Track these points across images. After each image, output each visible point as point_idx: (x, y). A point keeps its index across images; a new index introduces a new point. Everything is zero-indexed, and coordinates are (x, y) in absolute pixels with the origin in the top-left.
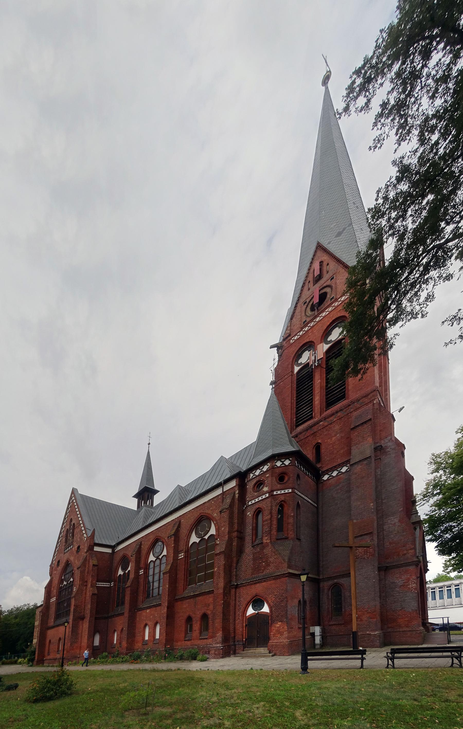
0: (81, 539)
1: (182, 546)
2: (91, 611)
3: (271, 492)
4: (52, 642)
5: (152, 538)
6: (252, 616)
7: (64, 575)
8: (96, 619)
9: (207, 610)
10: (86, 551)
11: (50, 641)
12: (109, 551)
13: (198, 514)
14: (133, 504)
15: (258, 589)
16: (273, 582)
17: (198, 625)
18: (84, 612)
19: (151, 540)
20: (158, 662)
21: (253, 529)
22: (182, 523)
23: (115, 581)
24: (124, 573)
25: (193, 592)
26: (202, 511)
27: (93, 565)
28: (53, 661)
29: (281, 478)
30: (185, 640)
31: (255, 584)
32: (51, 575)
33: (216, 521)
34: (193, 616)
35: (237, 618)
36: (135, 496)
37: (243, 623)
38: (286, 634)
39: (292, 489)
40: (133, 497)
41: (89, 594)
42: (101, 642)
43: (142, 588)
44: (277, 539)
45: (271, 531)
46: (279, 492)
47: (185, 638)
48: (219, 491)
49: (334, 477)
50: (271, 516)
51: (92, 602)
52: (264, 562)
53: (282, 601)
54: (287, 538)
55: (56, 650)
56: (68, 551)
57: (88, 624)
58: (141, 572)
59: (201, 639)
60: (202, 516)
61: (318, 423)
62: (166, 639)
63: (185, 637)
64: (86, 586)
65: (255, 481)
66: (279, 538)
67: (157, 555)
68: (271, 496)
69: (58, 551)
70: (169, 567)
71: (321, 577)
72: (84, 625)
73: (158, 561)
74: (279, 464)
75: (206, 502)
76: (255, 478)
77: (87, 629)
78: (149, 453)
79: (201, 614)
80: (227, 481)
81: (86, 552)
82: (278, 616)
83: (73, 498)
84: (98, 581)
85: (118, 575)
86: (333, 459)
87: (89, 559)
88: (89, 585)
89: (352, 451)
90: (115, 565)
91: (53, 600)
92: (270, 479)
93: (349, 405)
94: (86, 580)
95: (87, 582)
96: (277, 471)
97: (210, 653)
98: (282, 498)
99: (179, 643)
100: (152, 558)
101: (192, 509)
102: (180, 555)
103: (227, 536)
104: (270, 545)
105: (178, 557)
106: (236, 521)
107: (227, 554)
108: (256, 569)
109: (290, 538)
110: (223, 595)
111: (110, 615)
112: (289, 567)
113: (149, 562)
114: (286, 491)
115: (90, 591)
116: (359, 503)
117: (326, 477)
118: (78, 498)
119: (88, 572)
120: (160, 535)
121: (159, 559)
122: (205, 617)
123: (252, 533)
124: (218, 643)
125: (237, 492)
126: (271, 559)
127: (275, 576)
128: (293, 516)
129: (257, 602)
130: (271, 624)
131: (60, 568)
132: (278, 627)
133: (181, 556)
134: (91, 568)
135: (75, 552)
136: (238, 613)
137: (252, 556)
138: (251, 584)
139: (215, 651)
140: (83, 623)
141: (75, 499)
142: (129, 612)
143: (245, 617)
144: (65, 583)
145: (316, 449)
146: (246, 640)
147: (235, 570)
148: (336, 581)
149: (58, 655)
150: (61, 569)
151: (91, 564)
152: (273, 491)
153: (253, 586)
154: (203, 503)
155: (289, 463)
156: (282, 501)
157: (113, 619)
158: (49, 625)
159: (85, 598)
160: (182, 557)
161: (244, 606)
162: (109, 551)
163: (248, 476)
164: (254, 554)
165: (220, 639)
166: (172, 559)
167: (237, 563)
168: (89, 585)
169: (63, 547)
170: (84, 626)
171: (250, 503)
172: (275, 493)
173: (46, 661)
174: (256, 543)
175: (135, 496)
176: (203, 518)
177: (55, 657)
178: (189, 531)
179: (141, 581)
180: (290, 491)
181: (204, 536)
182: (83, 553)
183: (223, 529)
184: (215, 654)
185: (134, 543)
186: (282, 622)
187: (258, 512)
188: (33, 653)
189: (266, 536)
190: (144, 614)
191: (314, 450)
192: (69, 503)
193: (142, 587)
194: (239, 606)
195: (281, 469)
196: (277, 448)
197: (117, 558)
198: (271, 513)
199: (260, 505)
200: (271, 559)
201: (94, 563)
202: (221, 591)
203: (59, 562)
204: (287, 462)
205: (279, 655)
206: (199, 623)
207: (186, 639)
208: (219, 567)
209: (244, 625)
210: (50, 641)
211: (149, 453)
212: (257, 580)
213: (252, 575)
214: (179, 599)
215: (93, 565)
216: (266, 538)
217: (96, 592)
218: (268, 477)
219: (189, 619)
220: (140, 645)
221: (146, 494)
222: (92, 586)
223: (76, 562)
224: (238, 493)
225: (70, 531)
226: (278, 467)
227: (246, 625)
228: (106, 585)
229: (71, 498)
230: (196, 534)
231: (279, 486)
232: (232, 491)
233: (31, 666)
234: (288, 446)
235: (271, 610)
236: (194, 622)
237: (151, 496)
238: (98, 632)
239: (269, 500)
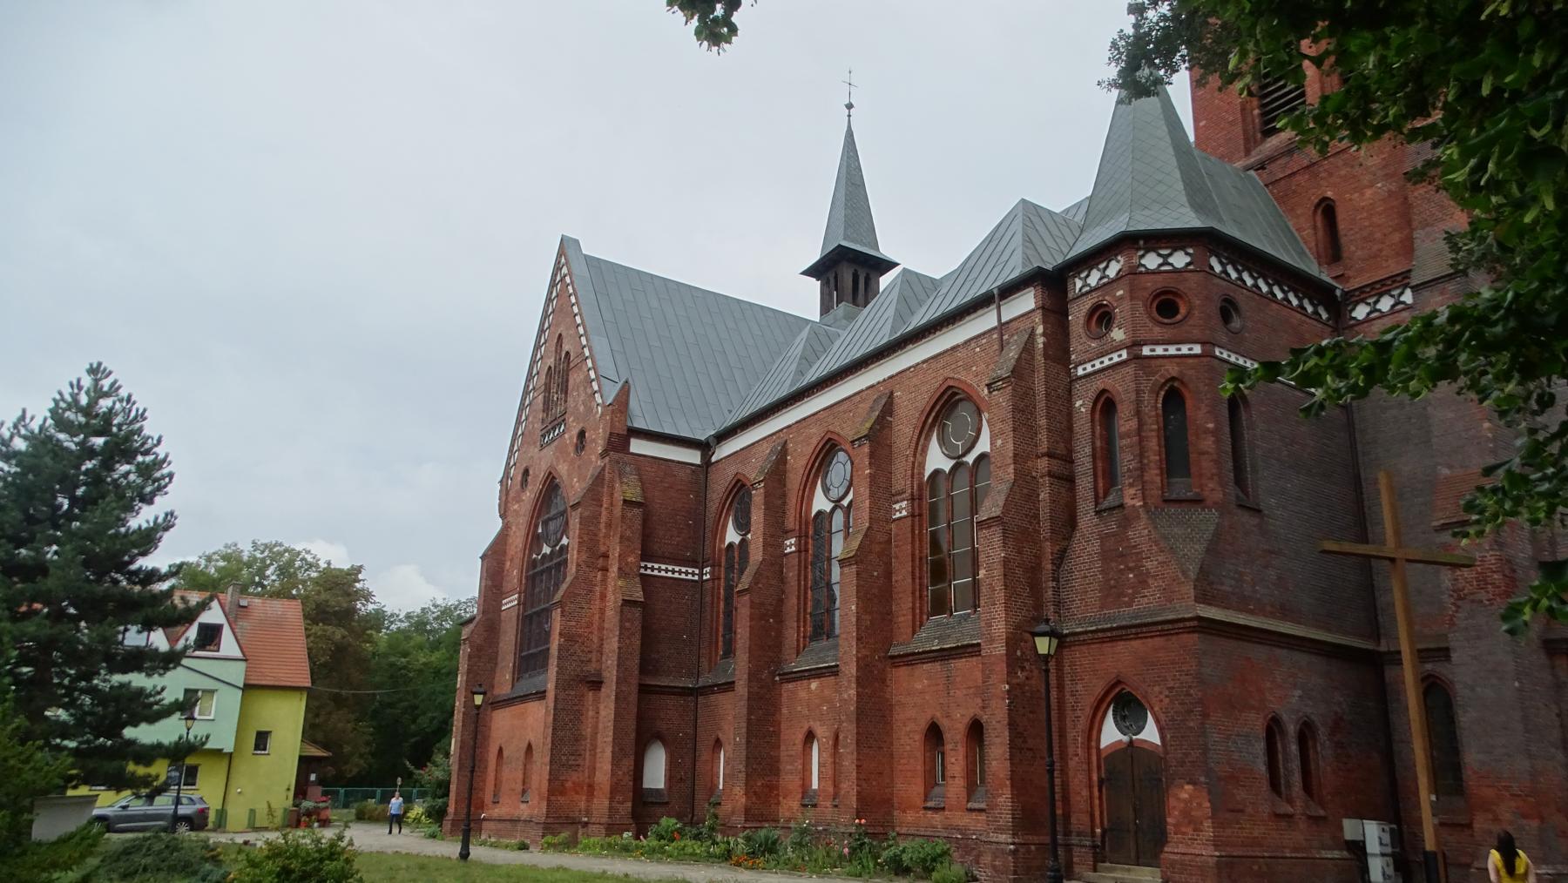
0: (589, 410)
1: (901, 480)
2: (620, 664)
3: (1134, 345)
4: (505, 753)
5: (815, 435)
7: (545, 523)
8: (644, 689)
10: (600, 450)
11: (501, 750)
12: (693, 457)
14: (805, 299)
15: (1122, 658)
16: (1159, 642)
17: (961, 757)
18: (599, 661)
19: (814, 441)
20: (817, 873)
21: (1094, 456)
22: (896, 400)
23: (715, 565)
25: (941, 638)
27: (625, 501)
28: (508, 825)
29: (1166, 305)
30: (926, 808)
31: (1112, 640)
32: (503, 515)
34: (944, 724)
35: (1071, 751)
36: (812, 272)
37: (1090, 771)
38: (1208, 830)
39: (1203, 343)
40: (804, 273)
41: (613, 601)
42: (670, 778)
43: (792, 602)
44: (1166, 501)
45: (1142, 469)
46: (1159, 350)
47: (925, 801)
48: (986, 321)
49: (1383, 315)
50: (1141, 424)
51: (622, 628)
52: (1131, 570)
53: (1190, 712)
54: (1198, 501)
55: (519, 787)
56: (553, 440)
57: (612, 706)
59: (971, 810)
60: (950, 387)
62: (859, 793)
63: (926, 798)
64: (605, 569)
65: (1087, 304)
66: (1174, 496)
67: (834, 494)
68: (1136, 358)
69: (520, 439)
70: (855, 544)
71: (1383, 648)
72: (602, 707)
74: (1151, 261)
76: (1087, 293)
77: (611, 724)
78: (850, 134)
79: (967, 720)
80: (1009, 290)
81: (603, 456)
82: (1182, 764)
83: (565, 270)
84: (647, 555)
86: (1376, 256)
87: (612, 481)
88: (614, 570)
89: (1417, 243)
90: (713, 506)
91: (510, 602)
92: (1126, 305)
94: (603, 549)
95: (605, 556)
96: (1151, 284)
98: (1173, 370)
99: (910, 816)
102: (897, 506)
103: (1011, 469)
104: (1143, 515)
105: (890, 511)
106: (1043, 422)
107: (1017, 526)
108: (1113, 592)
110: (1008, 666)
111: (706, 680)
112: (1203, 598)
114: (1185, 350)
115: (615, 589)
116: (1451, 415)
117: (1361, 312)
118: (580, 269)
119: (609, 525)
120: (837, 430)
121: (841, 507)
123: (1095, 468)
124: (999, 830)
125: (1040, 330)
126: (1149, 565)
128: (1214, 433)
129: (1129, 708)
131: (529, 495)
132: (1184, 801)
134: (618, 511)
135: (571, 449)
136: (1071, 735)
137: (1097, 544)
139: (995, 857)
140: (597, 701)
141: (570, 273)
142: (750, 680)
143: (1094, 751)
144: (546, 550)
145: (1324, 212)
146: (1104, 833)
147: (1051, 584)
149: (523, 806)
150: (537, 501)
151: (618, 497)
152: (1141, 344)
153: (1107, 647)
155: (1188, 264)
156: (1173, 379)
157: (713, 697)
158: (496, 692)
159: (602, 611)
160: (904, 513)
161: (1088, 711)
162: (693, 457)
163: (1070, 287)
164: (1103, 538)
166: (866, 516)
167: (1061, 557)
168: (614, 570)
169: (538, 426)
170: (603, 713)
171: (1080, 372)
172: (1146, 351)
173: (491, 825)
174: (1106, 504)
175: (812, 272)
177: (516, 813)
180: (1197, 349)
181: (964, 455)
182: (594, 458)
187: (1106, 406)
188: (443, 788)
189: (1131, 485)
190: (803, 694)
191: (1319, 218)
192: (553, 284)
193: (795, 601)
195: (1159, 277)
196: (1147, 212)
197: (719, 485)
198: (1138, 413)
200: (1149, 565)
201: (629, 496)
202: (1000, 649)
203: (526, 472)
204: (1179, 260)
206: (961, 750)
207: (929, 804)
209: (1095, 778)
210: (501, 750)
211: (850, 134)
213: (1102, 608)
215: (625, 501)
216: (1132, 491)
217: (639, 595)
218: (1121, 298)
219: (934, 734)
220: (795, 805)
221: (848, 270)
222: (622, 573)
223: (574, 487)
224: (1044, 334)
225: (555, 377)
226: (1149, 272)
227: (1101, 782)
228: (688, 573)
229: (558, 268)
231: (1157, 329)
232: (1022, 325)
233: (433, 836)
234: (1182, 210)
235: (1163, 738)
236: (948, 747)
237: (867, 280)
238: (660, 737)
239: (1130, 369)
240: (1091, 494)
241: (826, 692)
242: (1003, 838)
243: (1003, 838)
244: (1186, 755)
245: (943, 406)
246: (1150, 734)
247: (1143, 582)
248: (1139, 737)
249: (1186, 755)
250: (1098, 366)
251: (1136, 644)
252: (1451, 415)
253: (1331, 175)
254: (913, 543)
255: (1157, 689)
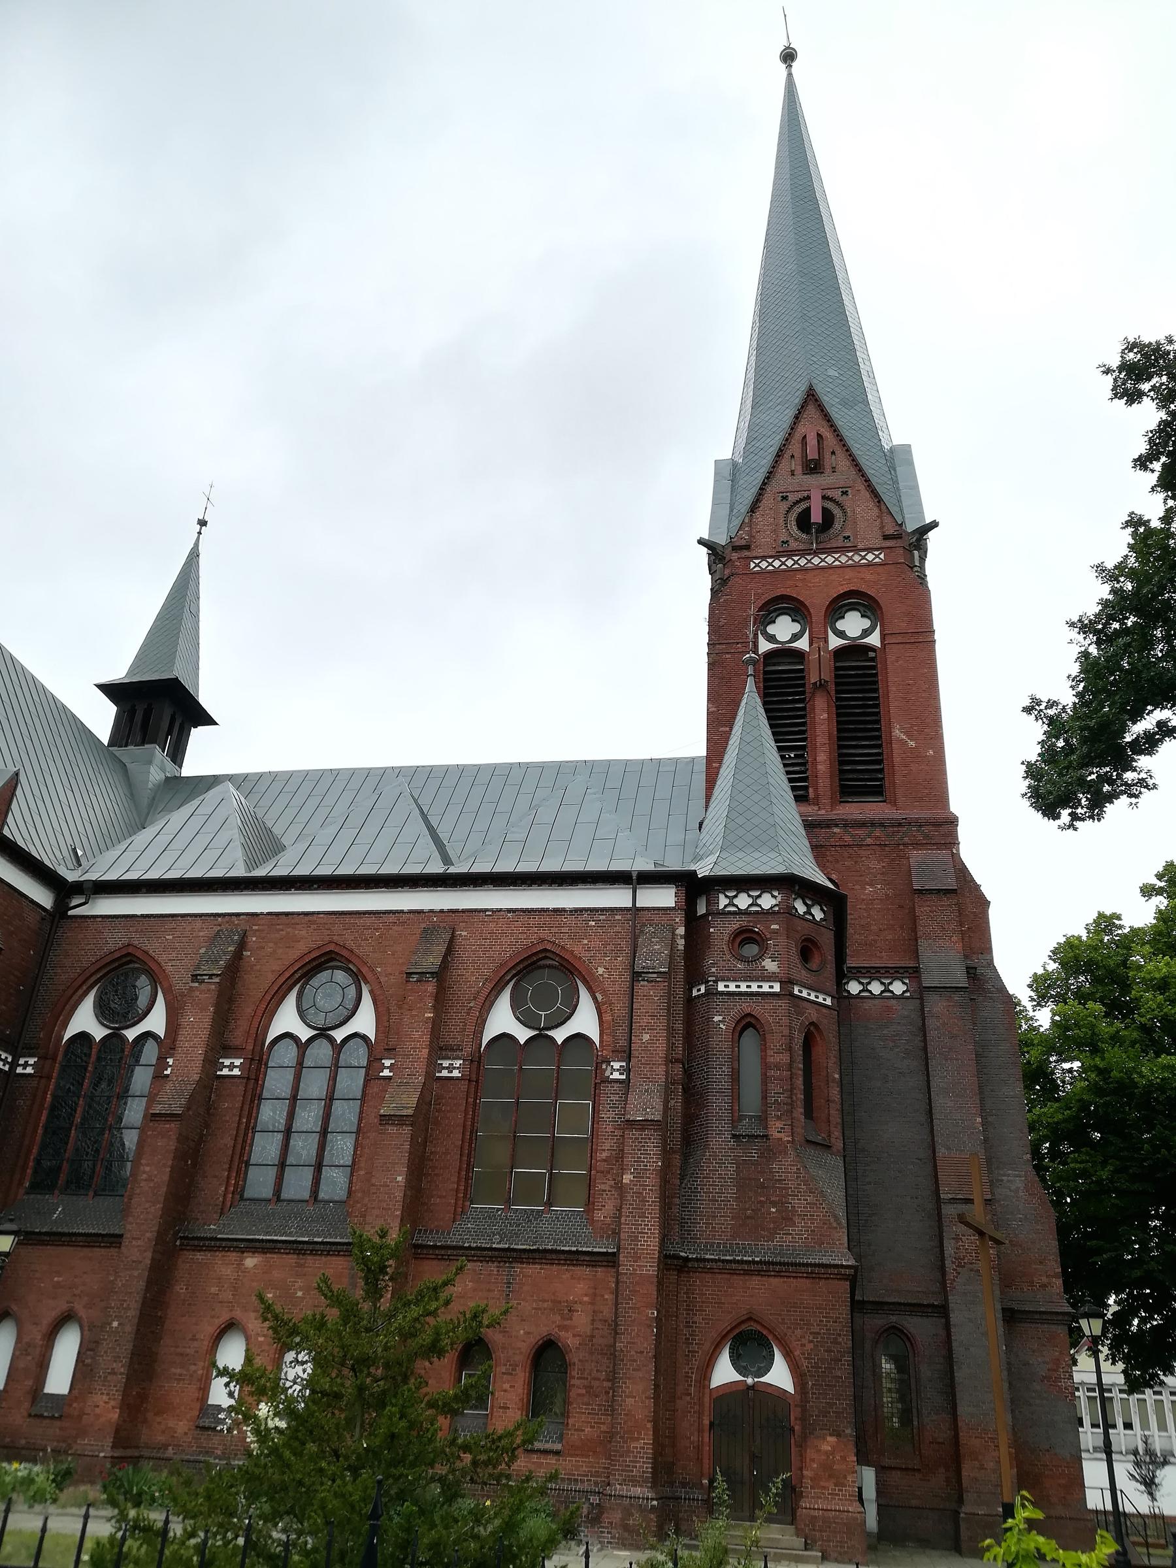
5: (306, 943)
6: (730, 1392)
9: (562, 1328)
12: (43, 897)
13: (534, 939)
15: (757, 1296)
16: (804, 1283)
23: (45, 1057)
24: (115, 1038)
26: (544, 934)
31: (747, 1273)
33: (604, 992)
48: (617, 898)
52: (774, 1204)
58: (232, 1067)
61: (828, 826)
65: (735, 924)
73: (321, 1053)
75: (564, 910)
78: (194, 556)
85: (69, 1034)
93: (900, 825)
97: (606, 1518)
100: (287, 1020)
101: (509, 911)
109: (834, 1150)
113: (271, 1036)
120: (350, 944)
121: (331, 1040)
122: (547, 1356)
124: (634, 1482)
127: (815, 1265)
129: (751, 1346)
130: (805, 1436)
132: (826, 1453)
133: (450, 1069)
137: (732, 1168)
138: (733, 1273)
139: (628, 1513)
143: (707, 1391)
148: (894, 1318)
153: (737, 1280)
154: (556, 910)
156: (812, 1023)
165: (644, 1466)
176: (546, 958)
178: (490, 986)
179: (229, 1107)
183: (646, 1037)
184: (626, 1528)
185: (198, 923)
186: (838, 1435)
187: (747, 1023)
189: (779, 1118)
194: (687, 1342)
199: (757, 1009)
204: (767, 901)
205: (837, 1561)
206: (522, 1376)
208: (638, 1175)
209: (706, 1422)
211: (194, 556)
212: (754, 1262)
214: (435, 1247)
216: (779, 1124)
218: (775, 932)
221: (158, 707)
227: (712, 1425)
230: (515, 1005)
240: (726, 1115)
241: (276, 1274)
242: (638, 1491)
243: (638, 1491)
244: (831, 1405)
245: (525, 968)
246: (779, 1376)
247: (787, 1218)
248: (762, 1380)
249: (831, 1405)
250: (743, 988)
251: (775, 1281)
252: (950, 1104)
253: (837, 861)
254: (466, 1113)
255: (798, 1332)
